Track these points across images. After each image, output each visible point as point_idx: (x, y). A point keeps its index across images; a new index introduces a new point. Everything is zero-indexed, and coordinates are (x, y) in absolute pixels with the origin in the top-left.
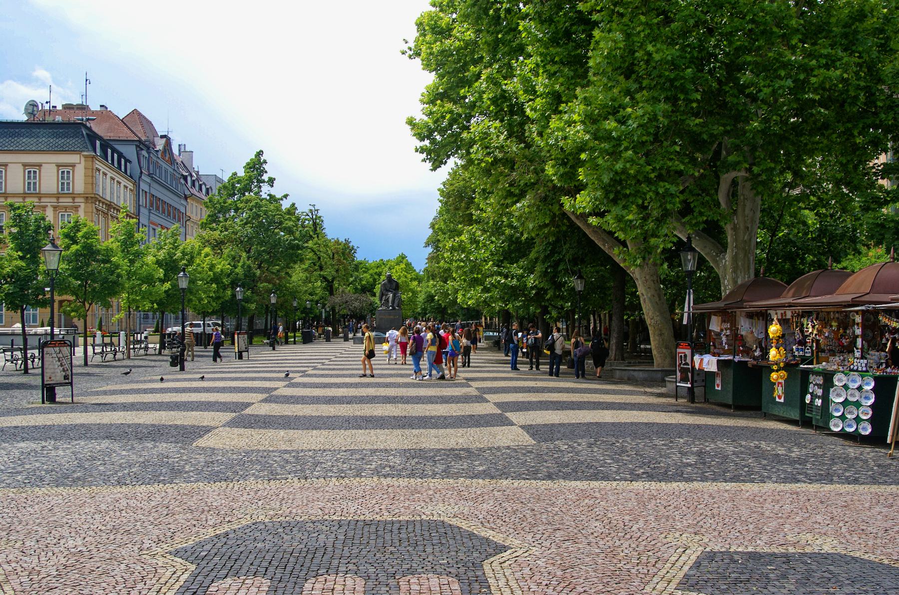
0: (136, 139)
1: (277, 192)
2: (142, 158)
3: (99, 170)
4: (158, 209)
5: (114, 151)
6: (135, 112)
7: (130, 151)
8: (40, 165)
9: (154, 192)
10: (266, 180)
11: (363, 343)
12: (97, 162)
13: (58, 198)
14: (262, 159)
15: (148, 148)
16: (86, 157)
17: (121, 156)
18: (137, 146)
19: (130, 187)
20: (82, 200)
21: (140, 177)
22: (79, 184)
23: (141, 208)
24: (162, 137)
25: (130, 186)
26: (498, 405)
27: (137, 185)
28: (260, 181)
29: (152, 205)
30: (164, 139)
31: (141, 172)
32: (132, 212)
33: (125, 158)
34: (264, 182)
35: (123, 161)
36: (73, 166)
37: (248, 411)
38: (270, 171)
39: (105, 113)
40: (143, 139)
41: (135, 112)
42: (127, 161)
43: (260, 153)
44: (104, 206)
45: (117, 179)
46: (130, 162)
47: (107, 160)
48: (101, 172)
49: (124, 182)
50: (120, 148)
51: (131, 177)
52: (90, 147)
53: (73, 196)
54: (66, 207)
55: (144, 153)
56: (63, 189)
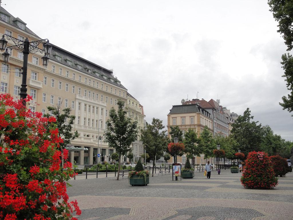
0: (212, 107)
1: (254, 120)
2: (214, 113)
3: (201, 117)
5: (206, 111)
8: (185, 117)
9: (218, 123)
14: (249, 111)
16: (197, 114)
21: (214, 119)
25: (211, 121)
28: (249, 118)
31: (214, 117)
33: (209, 113)
35: (208, 114)
36: (194, 116)
39: (203, 101)
42: (209, 114)
47: (204, 114)
49: (209, 120)
51: (211, 118)
52: (198, 111)
53: (194, 125)
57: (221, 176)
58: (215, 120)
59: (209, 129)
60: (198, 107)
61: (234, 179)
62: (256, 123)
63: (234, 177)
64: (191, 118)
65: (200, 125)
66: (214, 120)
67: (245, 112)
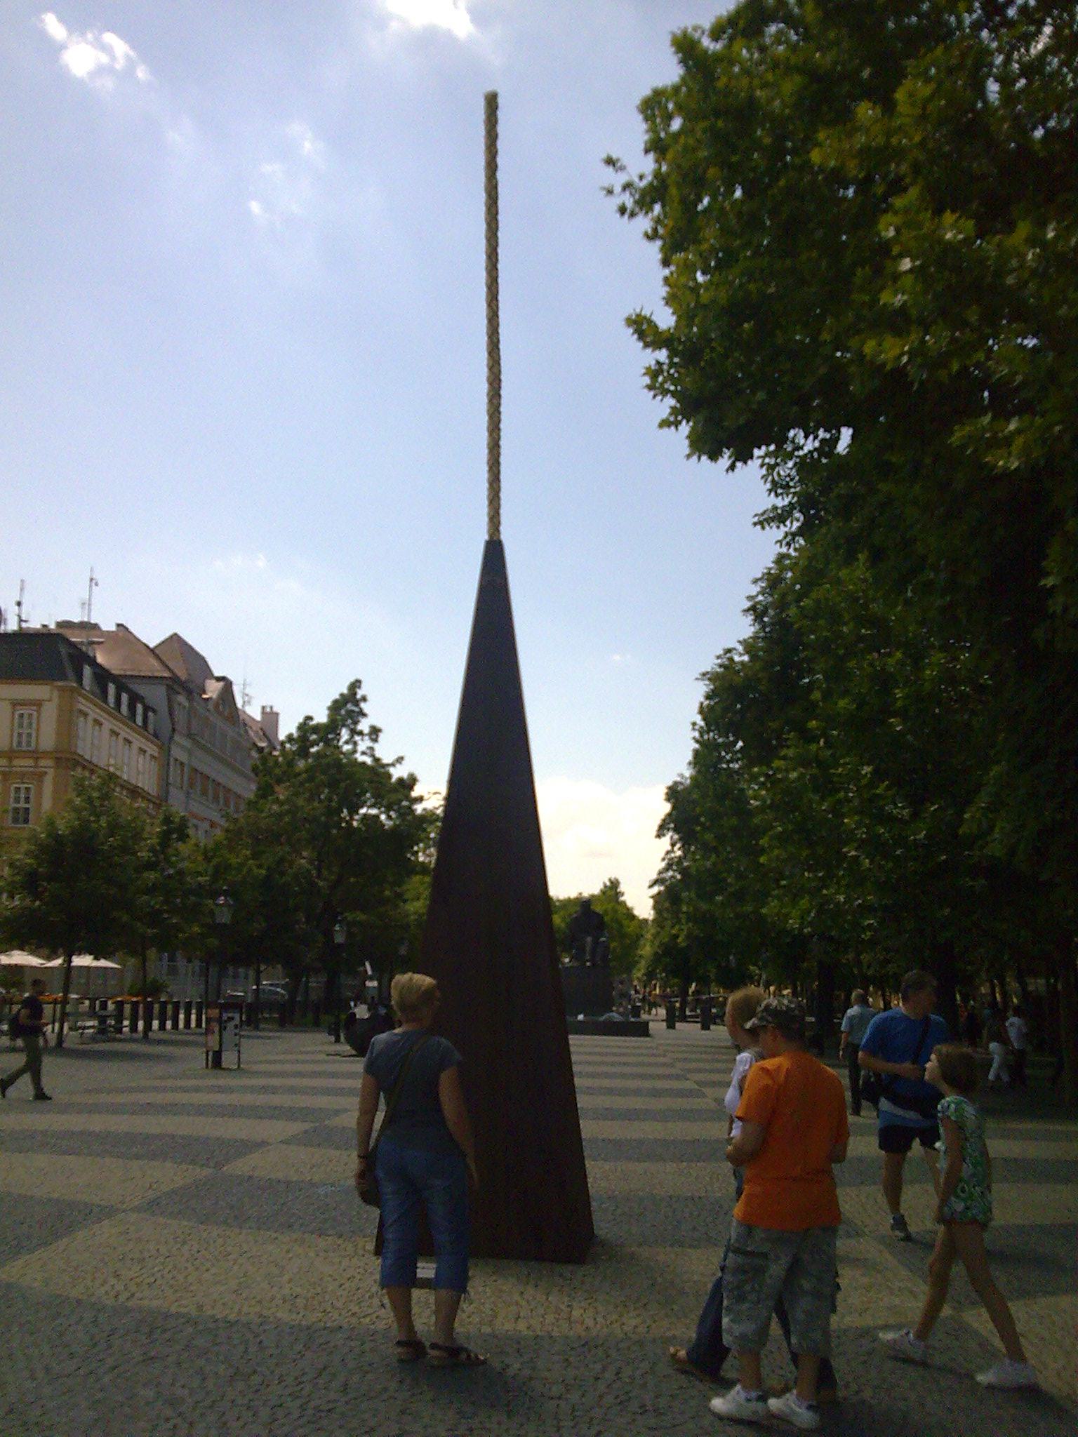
0: (166, 674)
1: (385, 752)
2: (176, 707)
3: (86, 715)
4: (204, 793)
6: (175, 639)
7: (158, 696)
10: (366, 730)
11: (364, 1056)
12: (81, 699)
13: (10, 759)
14: (360, 693)
15: (189, 693)
16: (61, 689)
17: (135, 699)
18: (169, 688)
19: (149, 752)
20: (50, 763)
21: (171, 738)
22: (47, 738)
23: (171, 789)
24: (219, 679)
25: (152, 750)
26: (697, 1083)
27: (165, 749)
28: (354, 732)
29: (191, 785)
30: (221, 684)
31: (174, 730)
32: (155, 794)
34: (361, 733)
36: (38, 704)
37: (240, 1167)
38: (374, 714)
40: (182, 675)
41: (175, 639)
43: (356, 685)
44: (125, 793)
45: (123, 734)
46: (154, 711)
47: (105, 700)
48: (90, 719)
49: (138, 741)
50: (142, 690)
52: (70, 672)
53: (36, 755)
54: (23, 775)
55: (181, 699)
56: (19, 743)
57: (75, 1122)
58: (179, 745)
59: (135, 792)
60: (70, 655)
61: (290, 1114)
62: (393, 765)
63: (293, 1090)
64: (22, 715)
65: (67, 759)
66: (173, 747)
67: (336, 707)
